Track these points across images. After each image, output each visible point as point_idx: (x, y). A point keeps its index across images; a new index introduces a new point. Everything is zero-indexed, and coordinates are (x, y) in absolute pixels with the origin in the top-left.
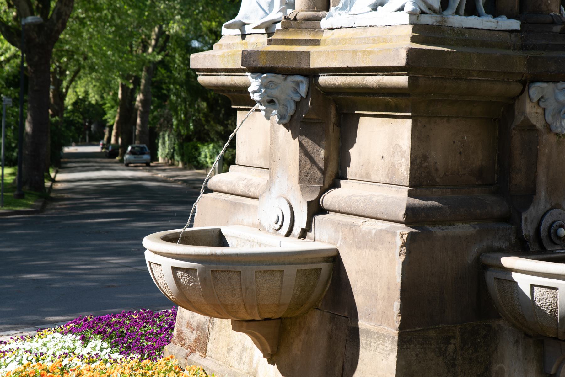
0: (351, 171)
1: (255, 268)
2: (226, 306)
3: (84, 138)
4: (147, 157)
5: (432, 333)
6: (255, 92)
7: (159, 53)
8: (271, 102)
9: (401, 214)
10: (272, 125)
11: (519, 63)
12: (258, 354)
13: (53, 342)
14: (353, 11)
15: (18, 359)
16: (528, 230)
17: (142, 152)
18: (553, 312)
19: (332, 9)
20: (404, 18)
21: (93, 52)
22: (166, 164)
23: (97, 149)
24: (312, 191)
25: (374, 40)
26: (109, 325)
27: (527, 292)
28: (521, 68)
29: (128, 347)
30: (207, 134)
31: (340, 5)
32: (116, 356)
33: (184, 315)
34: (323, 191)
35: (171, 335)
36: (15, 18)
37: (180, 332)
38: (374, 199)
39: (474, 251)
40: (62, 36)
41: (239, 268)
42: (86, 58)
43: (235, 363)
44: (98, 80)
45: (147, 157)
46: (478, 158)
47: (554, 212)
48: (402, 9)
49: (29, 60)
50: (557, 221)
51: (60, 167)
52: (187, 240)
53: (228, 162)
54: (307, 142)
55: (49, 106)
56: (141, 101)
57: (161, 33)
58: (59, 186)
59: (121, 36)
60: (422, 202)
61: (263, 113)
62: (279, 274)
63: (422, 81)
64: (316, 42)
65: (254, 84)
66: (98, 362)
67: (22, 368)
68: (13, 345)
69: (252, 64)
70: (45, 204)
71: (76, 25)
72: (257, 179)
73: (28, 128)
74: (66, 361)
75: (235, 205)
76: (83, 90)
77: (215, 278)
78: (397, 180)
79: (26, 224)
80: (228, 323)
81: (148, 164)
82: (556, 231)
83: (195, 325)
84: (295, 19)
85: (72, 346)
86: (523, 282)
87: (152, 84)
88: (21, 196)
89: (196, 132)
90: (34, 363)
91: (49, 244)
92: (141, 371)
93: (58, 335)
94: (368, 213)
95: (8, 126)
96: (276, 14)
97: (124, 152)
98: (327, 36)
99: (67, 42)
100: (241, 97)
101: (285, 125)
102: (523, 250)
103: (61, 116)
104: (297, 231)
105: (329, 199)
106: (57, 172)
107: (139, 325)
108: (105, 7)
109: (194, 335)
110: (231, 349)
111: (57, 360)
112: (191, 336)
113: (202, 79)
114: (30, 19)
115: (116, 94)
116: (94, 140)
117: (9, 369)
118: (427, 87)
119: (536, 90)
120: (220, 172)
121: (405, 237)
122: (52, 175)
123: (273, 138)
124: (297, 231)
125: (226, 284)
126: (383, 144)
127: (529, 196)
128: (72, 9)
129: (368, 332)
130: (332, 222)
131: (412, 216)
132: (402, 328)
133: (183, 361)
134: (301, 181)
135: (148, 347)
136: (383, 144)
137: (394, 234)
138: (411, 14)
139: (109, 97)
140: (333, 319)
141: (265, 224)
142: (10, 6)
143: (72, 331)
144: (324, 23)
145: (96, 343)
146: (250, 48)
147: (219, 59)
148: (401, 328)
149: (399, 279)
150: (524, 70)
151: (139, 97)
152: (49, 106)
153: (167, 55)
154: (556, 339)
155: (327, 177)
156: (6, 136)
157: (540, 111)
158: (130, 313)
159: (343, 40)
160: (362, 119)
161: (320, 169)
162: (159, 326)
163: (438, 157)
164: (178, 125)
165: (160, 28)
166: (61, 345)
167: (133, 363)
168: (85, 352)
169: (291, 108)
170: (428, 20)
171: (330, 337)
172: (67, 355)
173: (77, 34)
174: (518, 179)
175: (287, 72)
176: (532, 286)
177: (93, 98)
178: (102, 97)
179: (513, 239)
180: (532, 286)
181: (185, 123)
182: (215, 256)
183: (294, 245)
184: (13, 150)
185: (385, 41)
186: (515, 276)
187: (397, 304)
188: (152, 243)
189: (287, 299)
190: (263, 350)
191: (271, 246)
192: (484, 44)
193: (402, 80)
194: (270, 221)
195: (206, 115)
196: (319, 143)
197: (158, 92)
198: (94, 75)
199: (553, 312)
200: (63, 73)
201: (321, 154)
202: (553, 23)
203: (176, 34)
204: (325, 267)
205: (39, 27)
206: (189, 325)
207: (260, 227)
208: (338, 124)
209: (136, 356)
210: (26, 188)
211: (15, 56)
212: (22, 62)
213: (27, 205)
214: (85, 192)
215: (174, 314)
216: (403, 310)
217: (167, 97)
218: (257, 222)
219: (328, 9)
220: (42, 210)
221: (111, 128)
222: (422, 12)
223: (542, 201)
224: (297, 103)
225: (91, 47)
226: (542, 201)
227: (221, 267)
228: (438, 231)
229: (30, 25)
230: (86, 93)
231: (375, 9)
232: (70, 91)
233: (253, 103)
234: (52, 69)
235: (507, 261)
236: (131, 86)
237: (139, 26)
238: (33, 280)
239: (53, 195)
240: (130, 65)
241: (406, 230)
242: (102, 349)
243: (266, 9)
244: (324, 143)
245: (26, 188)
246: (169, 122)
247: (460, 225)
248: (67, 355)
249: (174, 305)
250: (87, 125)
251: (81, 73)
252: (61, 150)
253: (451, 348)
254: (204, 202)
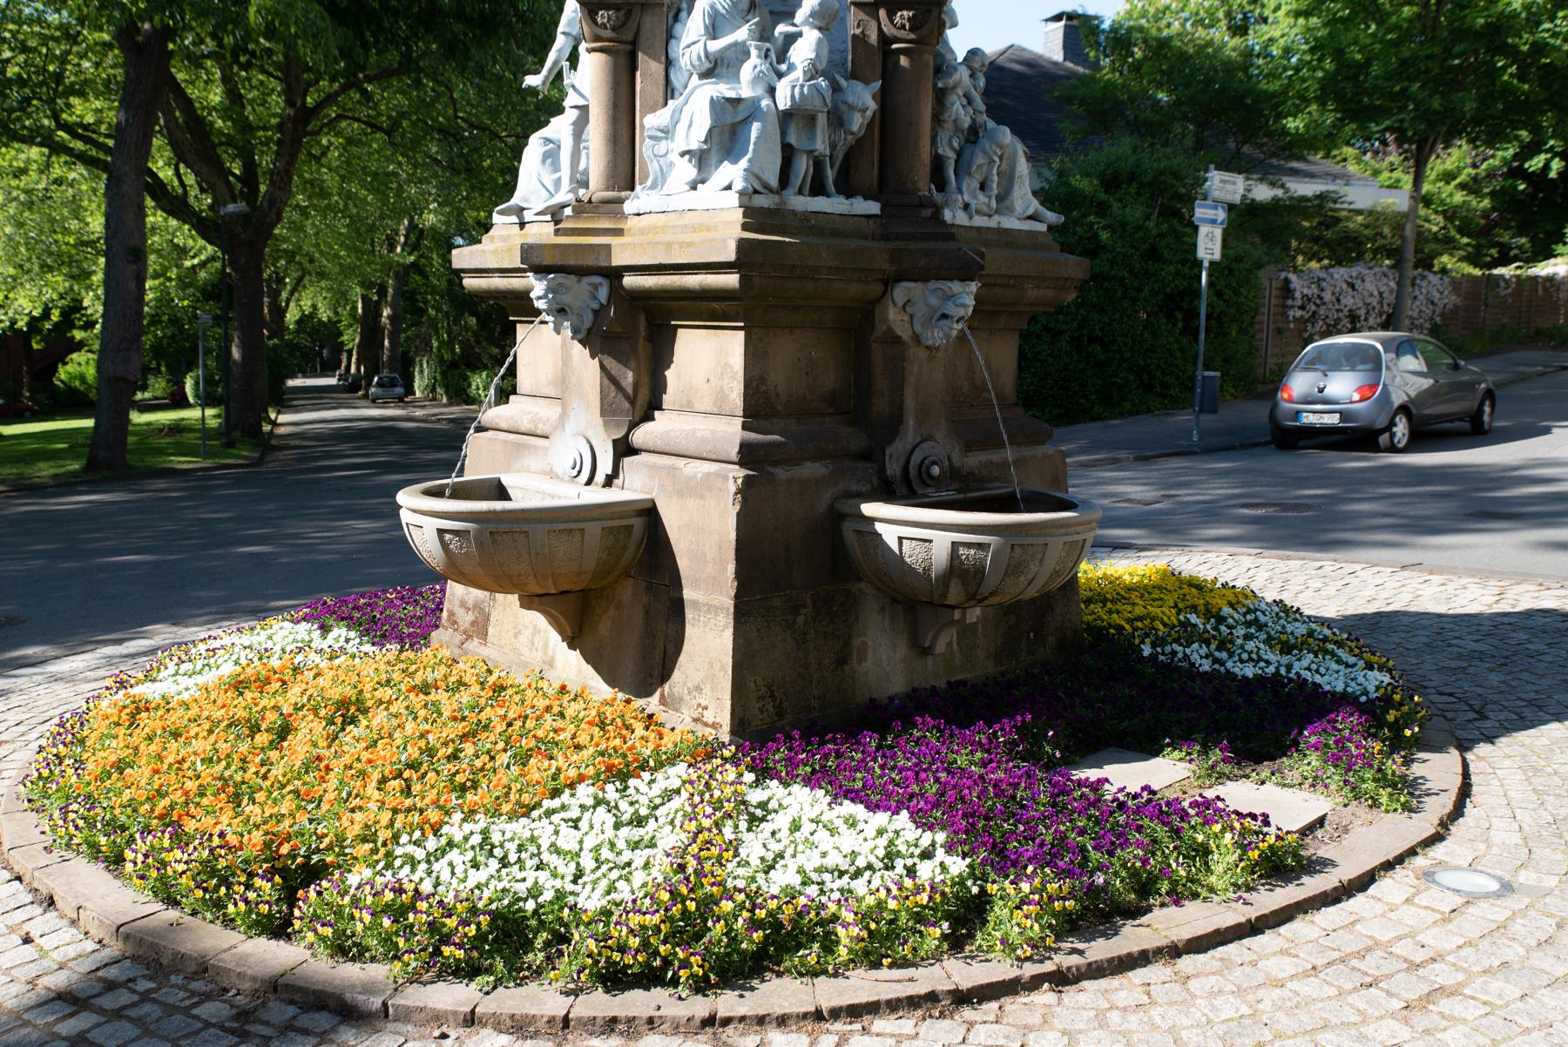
0: (668, 399)
1: (548, 526)
2: (510, 577)
3: (314, 367)
4: (399, 390)
5: (777, 602)
6: (539, 298)
7: (410, 254)
8: (561, 312)
9: (733, 452)
10: (564, 341)
11: (879, 256)
12: (554, 637)
13: (282, 633)
14: (666, 190)
15: (234, 657)
16: (893, 469)
17: (393, 384)
18: (927, 570)
19: (638, 188)
20: (733, 199)
21: (321, 252)
22: (426, 399)
23: (333, 381)
24: (618, 425)
25: (694, 229)
26: (356, 608)
27: (894, 546)
28: (882, 263)
29: (383, 636)
30: (479, 359)
31: (649, 183)
32: (368, 648)
33: (455, 590)
34: (633, 425)
35: (439, 618)
36: (211, 207)
37: (451, 614)
38: (699, 434)
39: (827, 496)
40: (277, 231)
41: (525, 527)
42: (312, 261)
43: (525, 651)
44: (329, 290)
45: (399, 390)
46: (830, 379)
47: (925, 445)
48: (729, 187)
49: (232, 264)
50: (908, 462)
51: (283, 405)
52: (459, 493)
53: (506, 393)
54: (611, 363)
55: (264, 324)
56: (389, 317)
57: (412, 227)
58: (282, 430)
59: (357, 231)
60: (760, 437)
61: (551, 325)
62: (578, 535)
63: (757, 281)
64: (618, 232)
65: (537, 287)
66: (343, 658)
67: (239, 669)
68: (227, 641)
69: (536, 261)
70: (263, 455)
71: (296, 216)
72: (545, 413)
73: (236, 353)
74: (300, 658)
75: (518, 446)
76: (309, 303)
77: (494, 541)
78: (727, 409)
79: (238, 482)
80: (514, 599)
81: (401, 400)
82: (928, 469)
83: (470, 603)
84: (590, 201)
85: (307, 638)
86: (889, 534)
87: (403, 294)
88: (230, 444)
89: (462, 356)
90: (257, 662)
91: (271, 506)
92: (402, 666)
93: (287, 624)
94: (691, 452)
95: (208, 352)
96: (564, 196)
97: (369, 385)
98: (632, 223)
99: (285, 240)
100: (520, 304)
101: (580, 341)
102: (888, 494)
103: (282, 338)
104: (600, 477)
105: (641, 435)
106: (279, 413)
107: (395, 606)
108: (335, 191)
109: (470, 617)
110: (520, 632)
111: (287, 656)
112: (465, 618)
113: (469, 282)
114: (231, 208)
115: (355, 308)
116: (328, 368)
117: (221, 671)
118: (764, 288)
119: (901, 292)
120: (497, 403)
121: (740, 481)
122: (273, 416)
123: (566, 359)
124: (600, 477)
125: (509, 548)
126: (708, 361)
127: (894, 425)
128: (290, 194)
129: (695, 603)
130: (646, 465)
131: (747, 456)
132: (739, 597)
133: (457, 651)
134: (603, 413)
135: (409, 635)
136: (708, 361)
137: (726, 478)
138: (741, 193)
139: (344, 312)
140: (649, 588)
141: (559, 470)
142: (202, 190)
143: (306, 618)
144: (628, 207)
145: (339, 633)
146: (530, 241)
147: (490, 256)
148: (737, 597)
149: (733, 535)
150: (886, 266)
151: (386, 312)
152: (264, 324)
153: (422, 256)
154: (931, 603)
155: (638, 407)
156: (205, 366)
157: (906, 318)
158: (385, 591)
159: (654, 229)
160: (680, 331)
161: (627, 396)
162: (423, 606)
163: (778, 379)
164: (439, 348)
165: (411, 220)
166: (291, 637)
167: (391, 656)
168: (325, 645)
169: (588, 319)
170: (763, 201)
171: (647, 612)
172: (300, 649)
173: (297, 228)
174: (880, 405)
175: (581, 272)
176: (900, 539)
177: (324, 314)
178: (336, 313)
179: (875, 481)
180: (900, 539)
181: (449, 345)
182: (494, 512)
183: (597, 495)
184: (217, 384)
185: (708, 229)
186: (879, 527)
187: (731, 567)
188: (409, 500)
189: (590, 564)
190: (561, 632)
191: (553, 497)
192: (835, 233)
193: (731, 280)
194: (564, 465)
195: (475, 334)
196: (625, 364)
197: (409, 305)
198: (323, 284)
199: (927, 570)
200: (280, 281)
201: (628, 378)
202: (922, 205)
203: (432, 228)
204: (638, 523)
205: (244, 218)
206: (463, 604)
207: (551, 474)
208: (650, 339)
209: (394, 647)
210: (237, 434)
211: (213, 259)
212: (224, 266)
213: (239, 457)
214: (318, 437)
215: (443, 591)
216: (739, 574)
217: (423, 312)
218: (547, 468)
219: (632, 188)
220: (259, 462)
221: (350, 352)
222: (756, 192)
223: (911, 432)
224: (595, 312)
225: (318, 245)
226: (911, 432)
227: (502, 528)
228: (781, 473)
229: (231, 215)
230: (314, 307)
231: (694, 188)
232: (292, 304)
233: (538, 312)
234: (265, 276)
235: (869, 509)
236: (375, 298)
237: (382, 217)
238: (251, 554)
239: (274, 442)
240: (373, 272)
241: (741, 473)
242: (347, 641)
243: (552, 189)
244: (632, 364)
245: (237, 434)
246: (428, 344)
247: (809, 464)
248: (300, 649)
249: (441, 579)
250: (317, 345)
251: (306, 281)
252: (284, 383)
253: (801, 619)
254: (475, 444)
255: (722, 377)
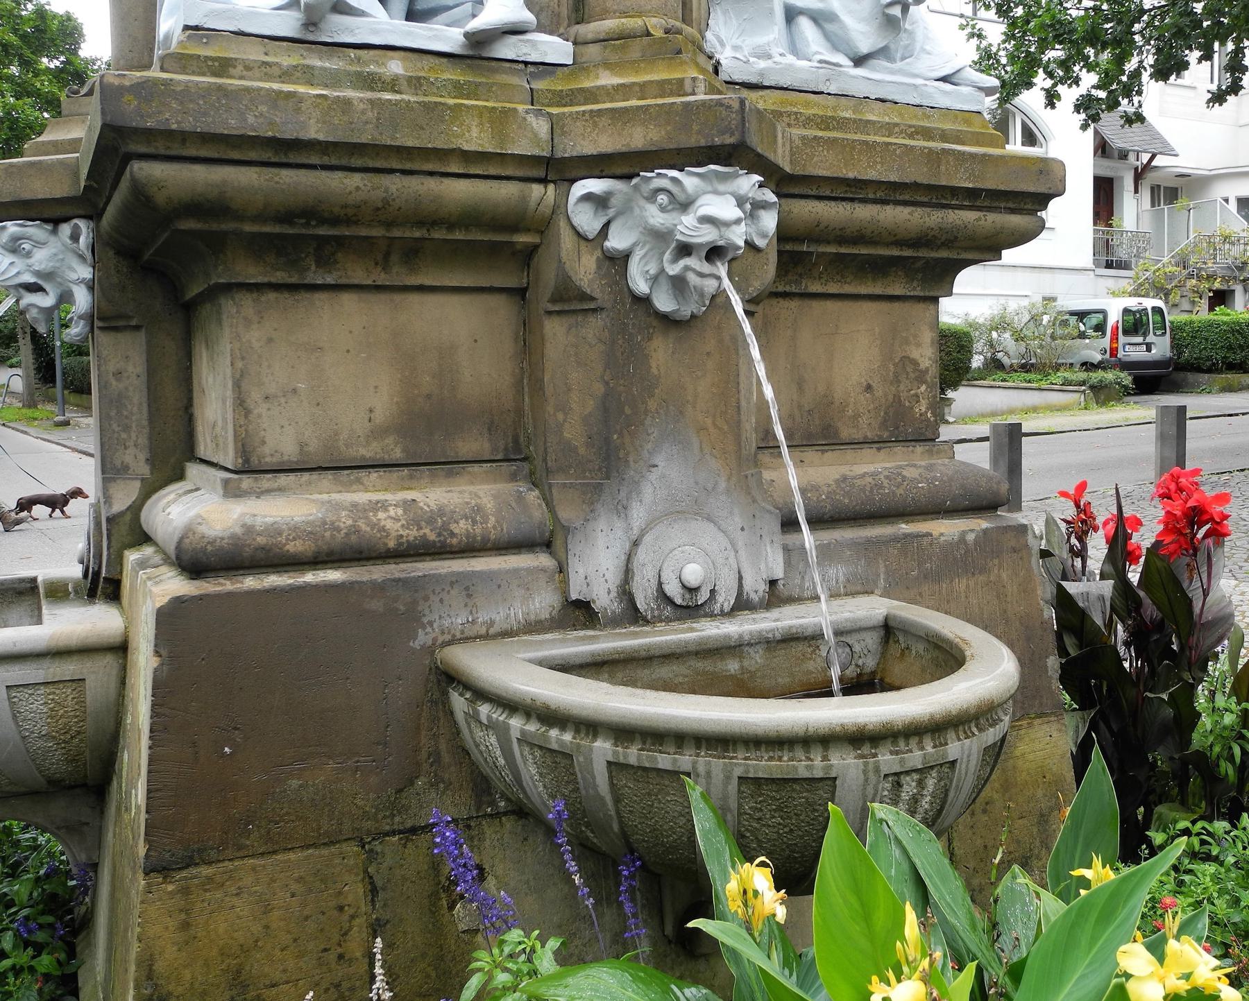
255: (897, 380)
